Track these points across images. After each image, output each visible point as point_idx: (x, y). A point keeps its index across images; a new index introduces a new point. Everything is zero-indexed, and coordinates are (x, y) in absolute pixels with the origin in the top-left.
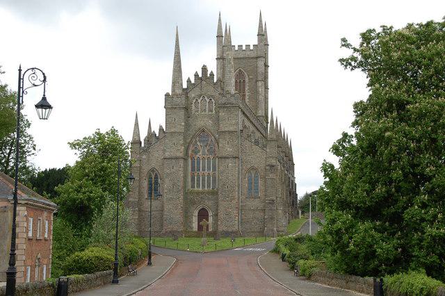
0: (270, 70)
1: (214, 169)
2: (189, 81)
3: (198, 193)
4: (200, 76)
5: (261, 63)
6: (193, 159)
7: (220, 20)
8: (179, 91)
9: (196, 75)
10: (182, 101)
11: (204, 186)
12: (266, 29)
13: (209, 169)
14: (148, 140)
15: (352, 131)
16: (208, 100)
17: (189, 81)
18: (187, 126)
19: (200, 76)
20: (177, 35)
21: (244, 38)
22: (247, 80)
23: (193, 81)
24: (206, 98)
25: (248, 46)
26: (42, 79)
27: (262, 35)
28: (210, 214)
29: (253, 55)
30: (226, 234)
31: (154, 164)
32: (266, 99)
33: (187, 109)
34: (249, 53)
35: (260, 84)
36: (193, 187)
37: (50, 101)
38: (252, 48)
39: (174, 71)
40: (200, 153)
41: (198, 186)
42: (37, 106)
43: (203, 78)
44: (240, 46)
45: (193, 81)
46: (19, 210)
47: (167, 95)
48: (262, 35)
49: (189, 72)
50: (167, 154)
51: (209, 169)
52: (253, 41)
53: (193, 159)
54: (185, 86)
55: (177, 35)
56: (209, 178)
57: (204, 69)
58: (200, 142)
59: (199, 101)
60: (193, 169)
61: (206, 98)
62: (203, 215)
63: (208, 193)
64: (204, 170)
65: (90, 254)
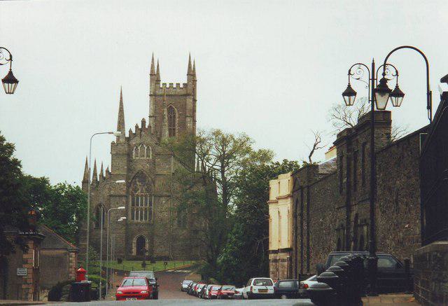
0: (198, 103)
1: (151, 204)
2: (130, 131)
3: (137, 224)
4: (140, 127)
5: (189, 101)
6: (133, 195)
7: (153, 59)
8: (122, 140)
9: (137, 127)
10: (125, 148)
11: (141, 218)
12: (194, 68)
13: (146, 205)
14: (95, 181)
15: (274, 160)
16: (146, 148)
17: (130, 131)
18: (129, 170)
19: (140, 127)
20: (121, 98)
21: (174, 76)
22: (177, 115)
23: (134, 132)
24: (145, 146)
25: (178, 84)
26: (395, 74)
27: (192, 74)
28: (147, 241)
29: (183, 92)
30: (160, 258)
31: (101, 200)
32: (194, 111)
33: (129, 155)
34: (178, 90)
35: (188, 119)
36: (133, 219)
37: (353, 87)
38: (182, 86)
39: (119, 123)
40: (139, 191)
41: (137, 219)
42: (344, 94)
43: (141, 130)
44: (171, 84)
45: (134, 132)
46: (275, 261)
47: (113, 144)
48: (192, 74)
49: (131, 125)
50: (112, 192)
51: (146, 205)
52: (183, 79)
53: (133, 195)
54: (127, 135)
55: (121, 98)
56: (146, 212)
57: (143, 122)
58: (139, 181)
59: (139, 148)
60: (133, 205)
61: (145, 146)
62: (141, 242)
63: (146, 224)
64: (142, 205)
65: (379, 219)
